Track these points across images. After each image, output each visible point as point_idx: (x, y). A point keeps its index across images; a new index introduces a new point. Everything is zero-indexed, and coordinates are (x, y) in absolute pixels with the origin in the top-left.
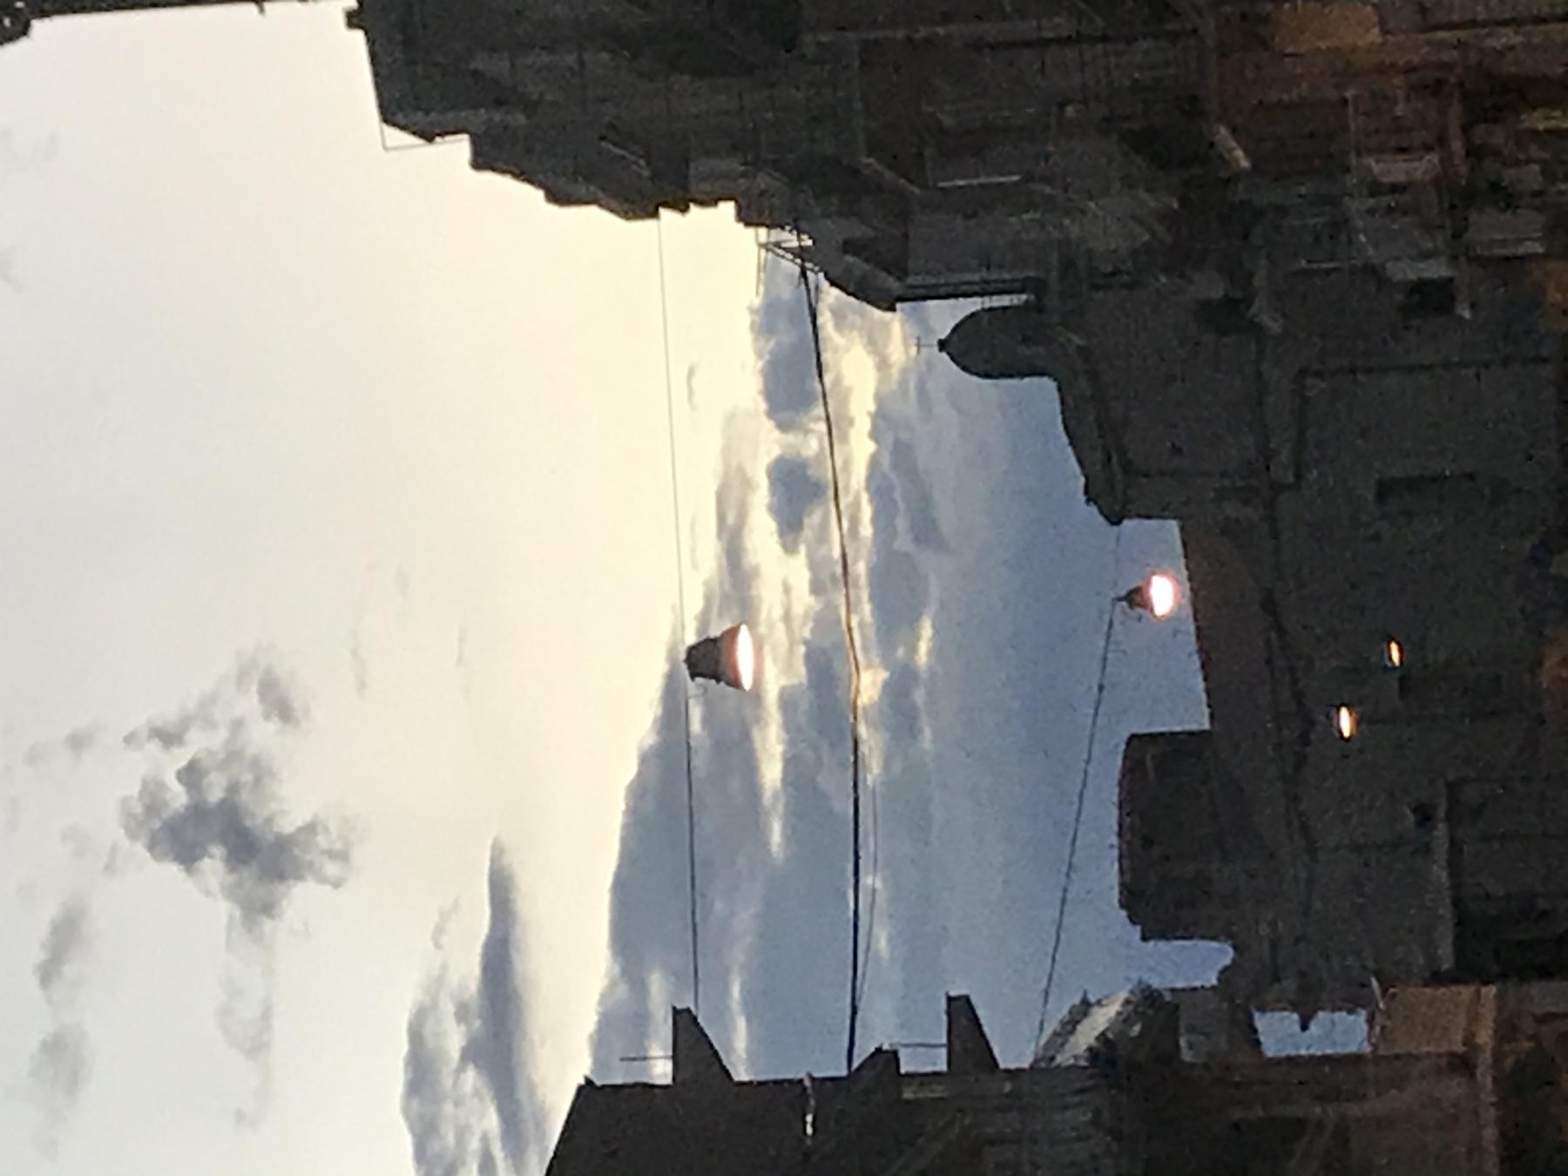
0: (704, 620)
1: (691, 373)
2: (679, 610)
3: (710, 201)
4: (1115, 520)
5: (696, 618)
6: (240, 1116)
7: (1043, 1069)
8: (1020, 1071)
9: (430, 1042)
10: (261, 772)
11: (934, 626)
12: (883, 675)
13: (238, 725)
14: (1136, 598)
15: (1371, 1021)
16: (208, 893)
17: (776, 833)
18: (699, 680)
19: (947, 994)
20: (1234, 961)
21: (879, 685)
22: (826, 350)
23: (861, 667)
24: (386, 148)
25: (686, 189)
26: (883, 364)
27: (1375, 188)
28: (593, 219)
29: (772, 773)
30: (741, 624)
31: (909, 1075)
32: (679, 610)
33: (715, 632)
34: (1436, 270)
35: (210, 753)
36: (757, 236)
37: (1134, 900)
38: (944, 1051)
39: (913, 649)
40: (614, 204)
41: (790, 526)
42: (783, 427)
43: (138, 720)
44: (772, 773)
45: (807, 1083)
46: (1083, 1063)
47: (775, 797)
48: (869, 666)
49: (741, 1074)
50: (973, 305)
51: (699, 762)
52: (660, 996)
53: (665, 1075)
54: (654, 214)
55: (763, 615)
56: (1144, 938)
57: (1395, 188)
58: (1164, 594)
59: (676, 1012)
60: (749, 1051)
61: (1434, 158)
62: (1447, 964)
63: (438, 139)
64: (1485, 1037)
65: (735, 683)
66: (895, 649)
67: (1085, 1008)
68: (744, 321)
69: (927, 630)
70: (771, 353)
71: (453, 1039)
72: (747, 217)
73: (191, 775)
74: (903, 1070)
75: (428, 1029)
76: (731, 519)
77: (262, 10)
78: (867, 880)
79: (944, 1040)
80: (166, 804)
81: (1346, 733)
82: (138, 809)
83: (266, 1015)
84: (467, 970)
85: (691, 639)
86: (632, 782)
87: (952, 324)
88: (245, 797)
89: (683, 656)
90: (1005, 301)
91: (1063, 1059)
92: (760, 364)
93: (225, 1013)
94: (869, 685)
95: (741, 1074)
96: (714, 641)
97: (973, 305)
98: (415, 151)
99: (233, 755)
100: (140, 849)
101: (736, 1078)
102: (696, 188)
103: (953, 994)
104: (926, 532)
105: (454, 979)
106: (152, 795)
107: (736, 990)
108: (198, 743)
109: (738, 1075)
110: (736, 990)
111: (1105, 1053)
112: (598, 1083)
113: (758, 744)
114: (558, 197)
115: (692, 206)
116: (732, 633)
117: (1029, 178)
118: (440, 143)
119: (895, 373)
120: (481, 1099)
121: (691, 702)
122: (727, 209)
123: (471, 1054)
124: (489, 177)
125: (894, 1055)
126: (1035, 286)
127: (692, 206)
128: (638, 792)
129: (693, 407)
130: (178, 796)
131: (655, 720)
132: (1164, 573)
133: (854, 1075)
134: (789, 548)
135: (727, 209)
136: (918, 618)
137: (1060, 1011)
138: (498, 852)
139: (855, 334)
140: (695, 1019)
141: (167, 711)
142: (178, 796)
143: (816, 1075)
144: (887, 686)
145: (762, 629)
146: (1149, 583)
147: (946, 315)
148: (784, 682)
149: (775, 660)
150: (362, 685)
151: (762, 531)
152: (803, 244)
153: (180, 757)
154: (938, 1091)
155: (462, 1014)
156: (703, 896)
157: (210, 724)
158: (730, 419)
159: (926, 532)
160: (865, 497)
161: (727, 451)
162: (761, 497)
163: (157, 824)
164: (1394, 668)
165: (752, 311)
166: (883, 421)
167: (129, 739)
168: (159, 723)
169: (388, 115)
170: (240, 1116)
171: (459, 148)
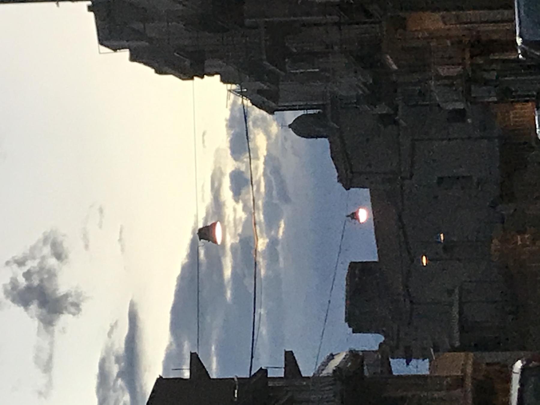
0: (206, 219)
1: (204, 134)
2: (197, 216)
3: (211, 74)
4: (348, 189)
5: (203, 219)
6: (40, 393)
7: (316, 379)
8: (308, 378)
9: (107, 369)
10: (52, 274)
11: (285, 224)
12: (267, 240)
13: (43, 258)
14: (354, 216)
15: (430, 362)
16: (31, 317)
17: (229, 294)
18: (202, 240)
19: (285, 350)
20: (384, 341)
21: (265, 245)
22: (249, 121)
23: (259, 238)
24: (100, 53)
25: (203, 70)
26: (269, 138)
27: (438, 77)
28: (171, 80)
29: (228, 273)
30: (218, 221)
31: (270, 378)
32: (197, 216)
33: (209, 224)
34: (460, 106)
35: (34, 267)
36: (227, 87)
37: (350, 319)
38: (283, 370)
39: (277, 232)
40: (177, 74)
41: (237, 193)
42: (236, 159)
43: (9, 258)
44: (228, 273)
45: (236, 380)
46: (331, 375)
47: (229, 282)
48: (262, 237)
49: (213, 376)
50: (301, 113)
51: (203, 269)
52: (187, 349)
53: (188, 376)
54: (192, 78)
55: (226, 219)
56: (353, 332)
57: (447, 77)
58: (364, 215)
59: (192, 354)
60: (217, 369)
61: (460, 68)
62: (457, 344)
63: (118, 51)
64: (469, 370)
65: (215, 242)
66: (271, 231)
67: (332, 357)
68: (223, 124)
69: (282, 225)
70: (233, 134)
71: (115, 369)
72: (224, 80)
73: (28, 275)
74: (269, 376)
75: (107, 364)
76: (216, 184)
77: (58, 4)
78: (258, 310)
79: (284, 366)
80: (18, 286)
81: (425, 264)
82: (9, 288)
83: (51, 357)
84: (120, 345)
85: (201, 226)
86: (179, 276)
87: (294, 119)
88: (46, 284)
89: (197, 232)
90: (311, 112)
91: (325, 373)
92: (229, 139)
93: (37, 358)
94: (262, 244)
95: (213, 376)
96: (208, 226)
97: (301, 113)
98: (111, 54)
99: (41, 269)
100: (9, 302)
101: (212, 377)
102: (207, 70)
103: (287, 350)
104: (285, 197)
105: (116, 347)
106: (14, 283)
107: (213, 348)
108: (31, 264)
109: (212, 375)
110: (213, 348)
111: (338, 370)
112: (164, 377)
113: (223, 263)
114: (159, 71)
115: (205, 76)
116: (214, 225)
117: (322, 70)
118: (119, 52)
119: (273, 137)
120: (123, 391)
121: (200, 248)
122: (217, 77)
123: (120, 374)
124: (135, 64)
125: (266, 371)
126: (322, 106)
127: (205, 76)
128: (182, 278)
129: (204, 146)
130: (22, 282)
131: (187, 256)
132: (362, 208)
133: (251, 377)
134: (237, 201)
135: (217, 77)
136: (279, 220)
137: (323, 359)
138: (132, 305)
139: (259, 129)
140: (198, 356)
141: (18, 252)
142: (22, 282)
143: (239, 377)
144: (268, 245)
145: (226, 223)
146: (358, 211)
147: (291, 116)
148: (233, 241)
149: (230, 234)
150: (87, 247)
151: (227, 194)
152: (243, 90)
153: (25, 269)
154: (281, 383)
155: (117, 360)
156: (202, 314)
157: (34, 258)
158: (217, 151)
159: (285, 197)
160: (262, 178)
161: (215, 162)
162: (227, 183)
163: (15, 292)
164: (440, 242)
165: (226, 120)
166: (269, 159)
167: (7, 263)
168: (16, 258)
169: (101, 42)
170: (40, 393)
171: (126, 53)
